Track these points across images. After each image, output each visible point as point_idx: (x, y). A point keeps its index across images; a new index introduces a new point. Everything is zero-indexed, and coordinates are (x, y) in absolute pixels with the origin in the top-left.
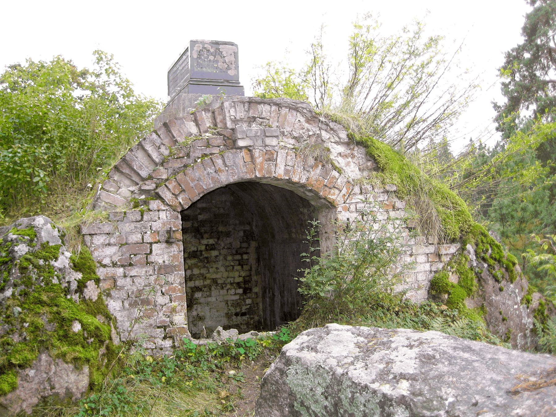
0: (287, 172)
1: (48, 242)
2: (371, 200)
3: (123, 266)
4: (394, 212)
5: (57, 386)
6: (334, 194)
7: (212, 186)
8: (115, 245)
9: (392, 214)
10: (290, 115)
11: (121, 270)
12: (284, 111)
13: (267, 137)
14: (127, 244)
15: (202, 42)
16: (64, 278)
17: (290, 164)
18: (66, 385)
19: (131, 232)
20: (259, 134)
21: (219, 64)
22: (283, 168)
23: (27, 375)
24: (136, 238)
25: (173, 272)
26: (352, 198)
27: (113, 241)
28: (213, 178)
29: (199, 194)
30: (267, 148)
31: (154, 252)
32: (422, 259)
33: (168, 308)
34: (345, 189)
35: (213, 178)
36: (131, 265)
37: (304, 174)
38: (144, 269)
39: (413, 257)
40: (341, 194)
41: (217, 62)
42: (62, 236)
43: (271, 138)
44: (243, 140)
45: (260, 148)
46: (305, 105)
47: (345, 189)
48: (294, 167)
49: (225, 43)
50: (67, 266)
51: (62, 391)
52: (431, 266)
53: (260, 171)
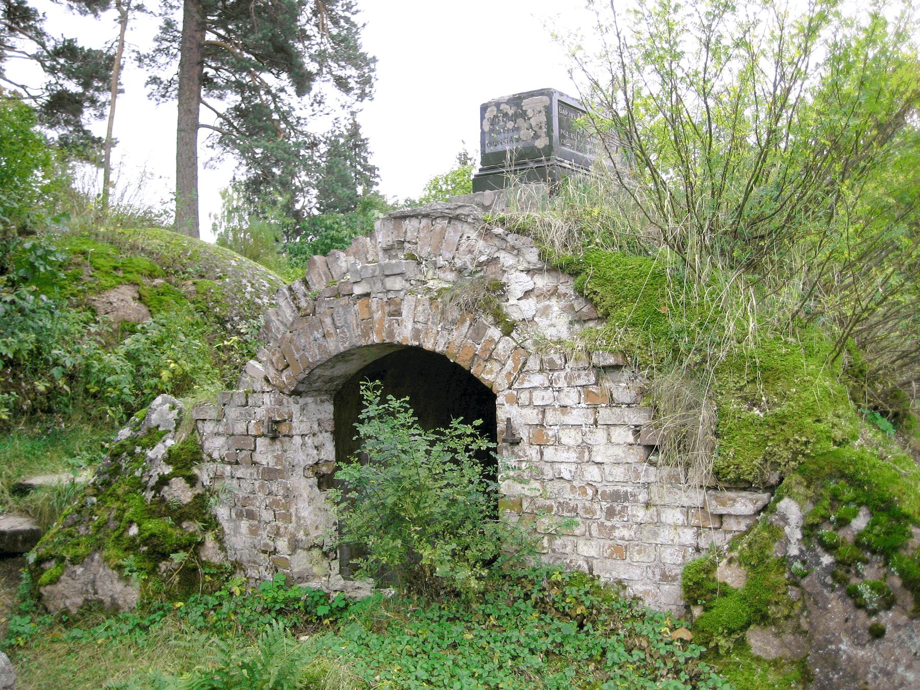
0: (416, 333)
1: (158, 426)
2: (562, 383)
3: (230, 463)
4: (608, 410)
5: (100, 591)
6: (491, 372)
7: (318, 357)
8: (223, 435)
9: (605, 414)
10: (450, 229)
11: (228, 468)
12: (441, 224)
13: (387, 276)
14: (233, 435)
15: (498, 104)
16: (149, 471)
17: (421, 319)
18: (111, 593)
19: (237, 420)
20: (377, 273)
21: (522, 132)
22: (409, 325)
23: (75, 572)
24: (240, 428)
25: (277, 479)
26: (523, 380)
27: (221, 429)
28: (320, 346)
29: (304, 370)
30: (390, 295)
31: (258, 450)
32: (673, 516)
33: (272, 527)
34: (510, 362)
35: (320, 346)
36: (237, 463)
37: (442, 336)
38: (249, 471)
39: (653, 510)
40: (504, 372)
41: (517, 129)
42: (178, 422)
43: (392, 278)
44: (359, 284)
45: (379, 295)
46: (467, 209)
47: (510, 362)
48: (426, 323)
49: (531, 94)
50: (160, 457)
51: (107, 600)
52: (698, 535)
53: (379, 333)
